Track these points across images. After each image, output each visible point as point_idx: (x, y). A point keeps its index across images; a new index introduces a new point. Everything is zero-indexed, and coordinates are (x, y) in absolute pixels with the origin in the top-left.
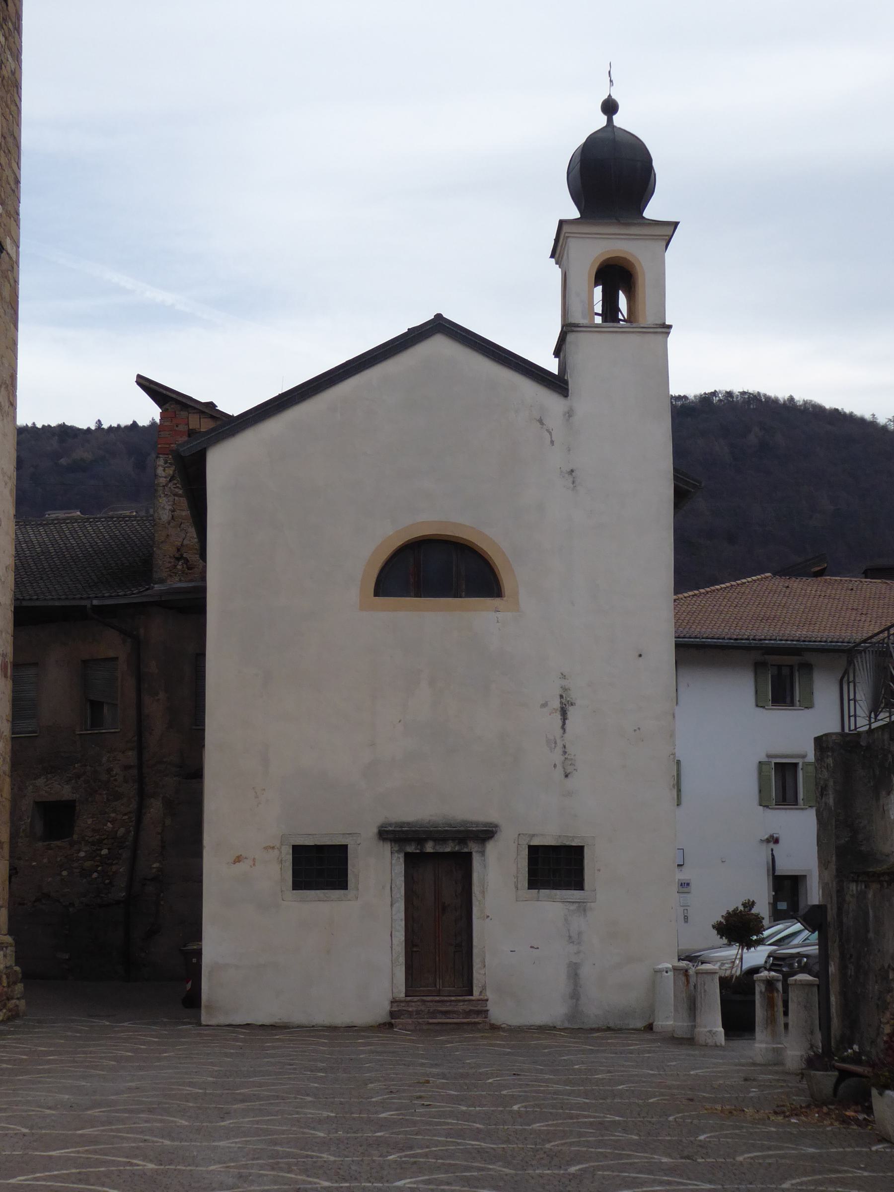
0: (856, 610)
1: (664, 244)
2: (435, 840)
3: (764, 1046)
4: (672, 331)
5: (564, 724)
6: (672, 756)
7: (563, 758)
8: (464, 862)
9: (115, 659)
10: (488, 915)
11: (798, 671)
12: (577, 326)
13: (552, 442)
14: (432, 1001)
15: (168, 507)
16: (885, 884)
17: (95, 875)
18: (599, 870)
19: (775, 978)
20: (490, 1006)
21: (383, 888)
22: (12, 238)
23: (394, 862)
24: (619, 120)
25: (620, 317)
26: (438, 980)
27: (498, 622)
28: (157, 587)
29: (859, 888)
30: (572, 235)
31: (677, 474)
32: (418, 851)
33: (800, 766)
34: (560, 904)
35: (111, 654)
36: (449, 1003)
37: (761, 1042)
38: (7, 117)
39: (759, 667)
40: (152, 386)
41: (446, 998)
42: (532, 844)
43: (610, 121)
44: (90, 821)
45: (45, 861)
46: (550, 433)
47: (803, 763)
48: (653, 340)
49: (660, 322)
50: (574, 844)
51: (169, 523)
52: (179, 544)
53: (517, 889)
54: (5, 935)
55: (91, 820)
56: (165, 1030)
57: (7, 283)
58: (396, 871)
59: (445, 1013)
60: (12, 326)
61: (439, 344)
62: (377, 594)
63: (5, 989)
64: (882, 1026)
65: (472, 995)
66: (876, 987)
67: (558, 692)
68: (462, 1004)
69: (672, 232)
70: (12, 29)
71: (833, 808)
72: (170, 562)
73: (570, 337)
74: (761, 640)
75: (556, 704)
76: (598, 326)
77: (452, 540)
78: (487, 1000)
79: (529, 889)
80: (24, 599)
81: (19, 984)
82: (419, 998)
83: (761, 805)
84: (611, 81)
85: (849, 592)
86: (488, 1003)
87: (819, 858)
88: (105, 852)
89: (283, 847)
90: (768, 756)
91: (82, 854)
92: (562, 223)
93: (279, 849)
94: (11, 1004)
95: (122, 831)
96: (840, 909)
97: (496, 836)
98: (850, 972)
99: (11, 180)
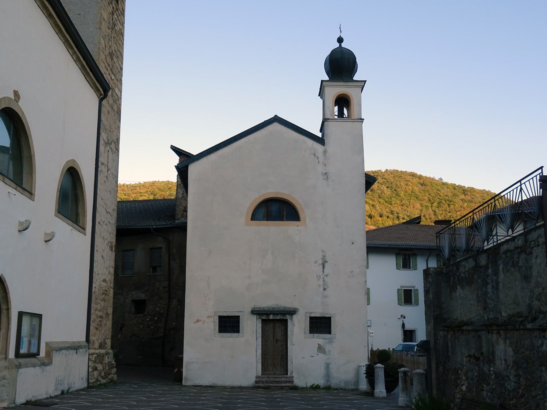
0: (432, 235)
1: (361, 89)
2: (274, 314)
3: (402, 399)
4: (364, 121)
5: (323, 270)
6: (365, 282)
7: (323, 283)
8: (285, 323)
9: (161, 248)
10: (294, 343)
11: (412, 256)
12: (329, 119)
13: (319, 162)
14: (272, 377)
15: (181, 193)
16: (456, 332)
17: (152, 327)
18: (337, 326)
19: (407, 371)
20: (294, 379)
21: (253, 333)
22: (118, 89)
23: (257, 322)
24: (343, 45)
25: (345, 116)
26: (274, 369)
27: (298, 230)
28: (176, 221)
29: (444, 334)
30: (326, 86)
31: (367, 179)
32: (267, 319)
33: (413, 290)
34: (322, 340)
35: (160, 246)
36: (278, 378)
37: (402, 397)
38: (117, 45)
39: (397, 255)
40: (176, 149)
41: (277, 376)
42: (311, 316)
43: (340, 45)
44: (151, 307)
45: (135, 322)
46: (318, 159)
47: (414, 289)
48: (357, 124)
49: (360, 118)
50: (327, 316)
51: (181, 198)
52: (185, 206)
53: (305, 334)
54: (109, 349)
55: (151, 307)
56: (166, 387)
57: (115, 105)
58: (258, 326)
59: (277, 382)
60: (118, 121)
61: (276, 126)
63: (108, 371)
64: (456, 394)
65: (287, 375)
66: (453, 377)
67: (322, 257)
68: (284, 378)
69: (364, 84)
70: (120, 14)
71: (432, 300)
72: (181, 212)
73: (326, 123)
74: (398, 245)
75: (320, 262)
76: (336, 119)
77: (281, 199)
78: (293, 377)
79: (310, 333)
80: (129, 226)
81: (114, 369)
82: (267, 376)
83: (399, 304)
84: (341, 31)
85: (429, 229)
86: (294, 378)
87: (426, 320)
88: (156, 318)
89: (215, 316)
90: (401, 287)
91: (148, 319)
92: (322, 81)
93: (214, 317)
94: (110, 377)
95: (162, 311)
96: (435, 343)
97: (297, 313)
98: (440, 370)
99: (119, 67)
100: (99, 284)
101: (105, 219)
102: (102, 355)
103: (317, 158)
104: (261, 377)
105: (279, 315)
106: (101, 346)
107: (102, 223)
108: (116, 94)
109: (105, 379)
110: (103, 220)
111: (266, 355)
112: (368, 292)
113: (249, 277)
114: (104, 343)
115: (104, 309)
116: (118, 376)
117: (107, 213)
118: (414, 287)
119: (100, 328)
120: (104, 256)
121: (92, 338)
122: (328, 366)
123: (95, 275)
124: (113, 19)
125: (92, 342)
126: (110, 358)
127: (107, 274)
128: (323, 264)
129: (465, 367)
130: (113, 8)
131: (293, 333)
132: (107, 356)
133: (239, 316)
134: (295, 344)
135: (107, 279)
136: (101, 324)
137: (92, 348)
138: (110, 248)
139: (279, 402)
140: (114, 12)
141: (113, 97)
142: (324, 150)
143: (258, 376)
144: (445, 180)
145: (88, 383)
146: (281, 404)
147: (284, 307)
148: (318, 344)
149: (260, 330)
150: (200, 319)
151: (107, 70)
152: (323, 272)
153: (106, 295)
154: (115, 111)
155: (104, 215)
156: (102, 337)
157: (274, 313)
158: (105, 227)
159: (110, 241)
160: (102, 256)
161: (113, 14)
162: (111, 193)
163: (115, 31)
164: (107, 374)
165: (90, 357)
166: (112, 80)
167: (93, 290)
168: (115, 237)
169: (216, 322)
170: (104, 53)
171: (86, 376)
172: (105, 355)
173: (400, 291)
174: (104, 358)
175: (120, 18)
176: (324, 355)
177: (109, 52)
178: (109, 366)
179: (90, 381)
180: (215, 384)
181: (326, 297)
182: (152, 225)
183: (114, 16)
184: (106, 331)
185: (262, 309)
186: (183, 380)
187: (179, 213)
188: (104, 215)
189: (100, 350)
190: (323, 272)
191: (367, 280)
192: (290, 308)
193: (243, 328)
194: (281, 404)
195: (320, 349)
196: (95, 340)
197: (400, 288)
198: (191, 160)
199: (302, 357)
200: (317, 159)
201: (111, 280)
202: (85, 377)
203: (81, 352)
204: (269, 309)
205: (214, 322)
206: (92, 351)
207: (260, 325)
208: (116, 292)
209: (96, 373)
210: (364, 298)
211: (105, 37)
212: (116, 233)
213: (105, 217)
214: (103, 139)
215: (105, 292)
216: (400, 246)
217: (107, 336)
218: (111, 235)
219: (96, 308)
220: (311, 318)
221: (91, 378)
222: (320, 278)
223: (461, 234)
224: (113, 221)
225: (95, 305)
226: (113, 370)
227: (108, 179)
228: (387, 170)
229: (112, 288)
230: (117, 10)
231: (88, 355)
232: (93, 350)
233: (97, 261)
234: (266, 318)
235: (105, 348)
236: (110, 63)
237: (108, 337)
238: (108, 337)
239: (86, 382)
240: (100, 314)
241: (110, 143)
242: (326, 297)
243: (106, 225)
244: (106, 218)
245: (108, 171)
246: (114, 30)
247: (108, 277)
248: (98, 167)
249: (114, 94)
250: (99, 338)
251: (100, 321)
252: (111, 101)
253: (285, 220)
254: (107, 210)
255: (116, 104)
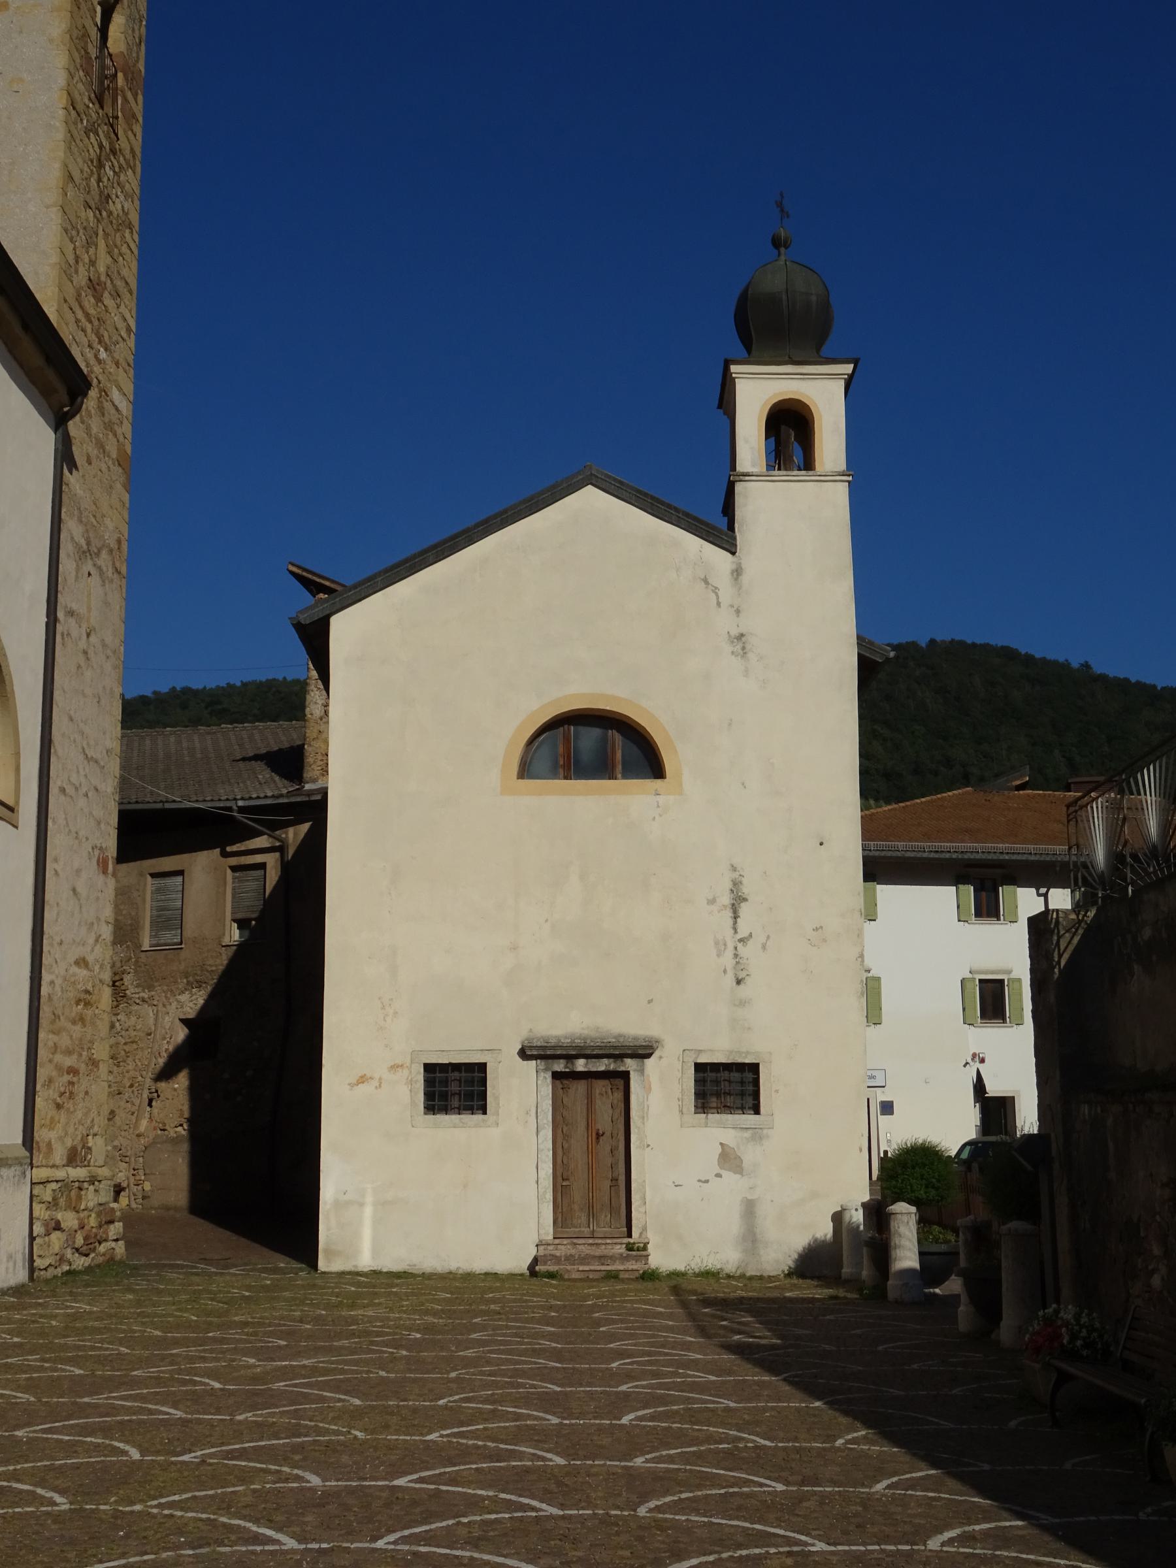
5: (735, 923)
13: (719, 604)
18: (777, 1091)
23: (539, 1082)
50: (747, 1061)
51: (321, 719)
57: (111, 436)
62: (526, 770)
63: (94, 1230)
67: (729, 885)
75: (726, 899)
80: (167, 802)
83: (964, 1023)
93: (410, 1068)
100: (63, 972)
101: (83, 780)
102: (77, 1184)
103: (713, 591)
104: (553, 1244)
105: (605, 1061)
106: (74, 1158)
107: (70, 790)
108: (114, 405)
109: (87, 1255)
110: (74, 779)
111: (567, 1179)
112: (872, 990)
113: (514, 948)
114: (83, 1147)
115: (82, 1048)
116: (129, 1245)
117: (86, 762)
118: (1009, 972)
119: (69, 1105)
120: (79, 890)
121: (40, 1134)
122: (749, 1209)
123: (51, 945)
124: (99, 180)
125: (43, 1146)
126: (102, 1193)
127: (91, 941)
128: (733, 905)
129: (1158, 1218)
130: (101, 146)
131: (647, 1113)
132: (92, 1188)
133: (485, 1064)
134: (652, 1146)
135: (90, 959)
136: (71, 1093)
137: (44, 1163)
138: (98, 864)
139: (598, 1323)
140: (102, 158)
141: (103, 415)
142: (734, 567)
143: (544, 1242)
144: (1098, 668)
145: (32, 1270)
146: (601, 1329)
147: (620, 1036)
148: (721, 1144)
149: (547, 1105)
150: (368, 1075)
151: (84, 330)
152: (735, 931)
153: (87, 1004)
154: (109, 456)
155: (77, 768)
156: (76, 1129)
157: (589, 1052)
158: (82, 802)
159: (99, 845)
160: (74, 890)
161: (101, 166)
162: (98, 702)
163: (109, 217)
164: (92, 1242)
165: (35, 1192)
166: (99, 361)
167: (45, 990)
168: (114, 834)
169: (416, 1082)
170: (72, 282)
171: (25, 1248)
172: (86, 1185)
173: (968, 985)
174: (83, 1193)
175: (122, 177)
176: (740, 1176)
177: (90, 280)
178: (99, 1214)
179: (38, 1263)
180: (415, 1265)
181: (742, 1003)
182: (235, 799)
183: (102, 171)
184: (90, 1110)
185: (553, 1042)
186: (320, 1256)
187: (315, 762)
188: (77, 768)
189: (70, 1169)
190: (735, 931)
191: (865, 954)
192: (636, 1038)
193: (497, 1098)
194: (601, 1329)
195: (729, 1159)
196: (53, 1140)
197: (970, 976)
198: (338, 599)
199: (674, 1182)
200: (714, 595)
201: (103, 960)
202: (21, 1251)
203: (5, 1178)
204: (573, 1042)
205: (411, 1080)
206: (40, 1174)
207: (547, 1089)
208: (134, 995)
209: (59, 1239)
210: (855, 1007)
211: (74, 233)
212: (117, 820)
213: (82, 773)
214: (72, 538)
215: (83, 996)
216: (969, 854)
217: (92, 1127)
218: (102, 825)
219: (55, 1044)
220: (700, 1068)
221: (41, 1253)
222: (725, 949)
223: (1137, 809)
224: (109, 786)
225: (51, 1036)
226: (112, 1227)
227: (88, 659)
228: (932, 642)
229: (108, 985)
230: (113, 152)
231: (29, 1184)
232: (49, 1169)
233: (58, 904)
234: (566, 1067)
235: (86, 1163)
236: (92, 311)
237: (96, 1129)
238: (96, 1129)
239: (24, 1264)
240: (69, 1062)
241: (96, 551)
242: (742, 1003)
243: (86, 795)
244: (86, 776)
245: (88, 635)
246: (104, 214)
247: (92, 950)
248: (56, 620)
249: (107, 405)
250: (66, 1134)
251: (71, 1083)
252: (96, 425)
253: (619, 776)
254: (87, 752)
255: (115, 435)
